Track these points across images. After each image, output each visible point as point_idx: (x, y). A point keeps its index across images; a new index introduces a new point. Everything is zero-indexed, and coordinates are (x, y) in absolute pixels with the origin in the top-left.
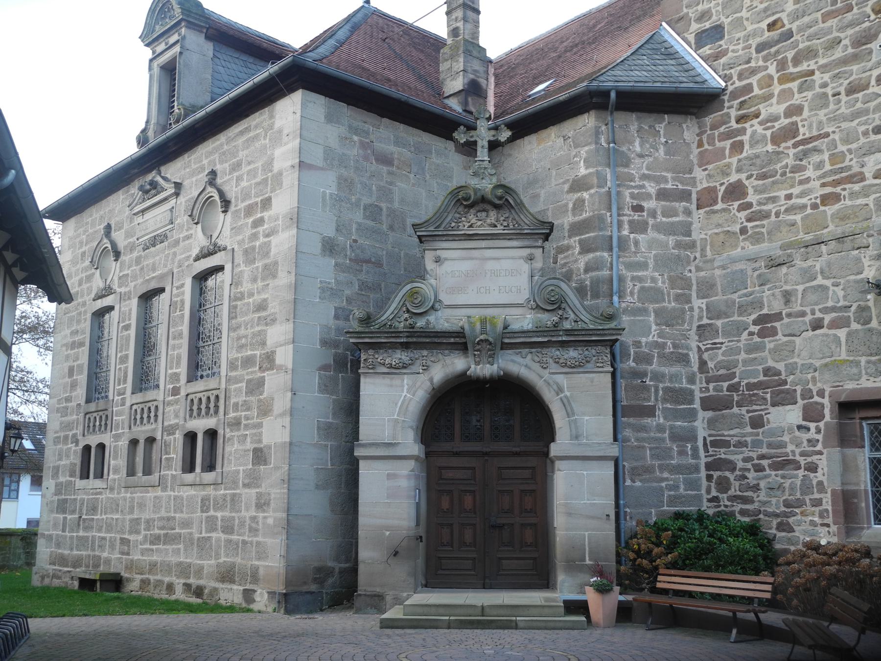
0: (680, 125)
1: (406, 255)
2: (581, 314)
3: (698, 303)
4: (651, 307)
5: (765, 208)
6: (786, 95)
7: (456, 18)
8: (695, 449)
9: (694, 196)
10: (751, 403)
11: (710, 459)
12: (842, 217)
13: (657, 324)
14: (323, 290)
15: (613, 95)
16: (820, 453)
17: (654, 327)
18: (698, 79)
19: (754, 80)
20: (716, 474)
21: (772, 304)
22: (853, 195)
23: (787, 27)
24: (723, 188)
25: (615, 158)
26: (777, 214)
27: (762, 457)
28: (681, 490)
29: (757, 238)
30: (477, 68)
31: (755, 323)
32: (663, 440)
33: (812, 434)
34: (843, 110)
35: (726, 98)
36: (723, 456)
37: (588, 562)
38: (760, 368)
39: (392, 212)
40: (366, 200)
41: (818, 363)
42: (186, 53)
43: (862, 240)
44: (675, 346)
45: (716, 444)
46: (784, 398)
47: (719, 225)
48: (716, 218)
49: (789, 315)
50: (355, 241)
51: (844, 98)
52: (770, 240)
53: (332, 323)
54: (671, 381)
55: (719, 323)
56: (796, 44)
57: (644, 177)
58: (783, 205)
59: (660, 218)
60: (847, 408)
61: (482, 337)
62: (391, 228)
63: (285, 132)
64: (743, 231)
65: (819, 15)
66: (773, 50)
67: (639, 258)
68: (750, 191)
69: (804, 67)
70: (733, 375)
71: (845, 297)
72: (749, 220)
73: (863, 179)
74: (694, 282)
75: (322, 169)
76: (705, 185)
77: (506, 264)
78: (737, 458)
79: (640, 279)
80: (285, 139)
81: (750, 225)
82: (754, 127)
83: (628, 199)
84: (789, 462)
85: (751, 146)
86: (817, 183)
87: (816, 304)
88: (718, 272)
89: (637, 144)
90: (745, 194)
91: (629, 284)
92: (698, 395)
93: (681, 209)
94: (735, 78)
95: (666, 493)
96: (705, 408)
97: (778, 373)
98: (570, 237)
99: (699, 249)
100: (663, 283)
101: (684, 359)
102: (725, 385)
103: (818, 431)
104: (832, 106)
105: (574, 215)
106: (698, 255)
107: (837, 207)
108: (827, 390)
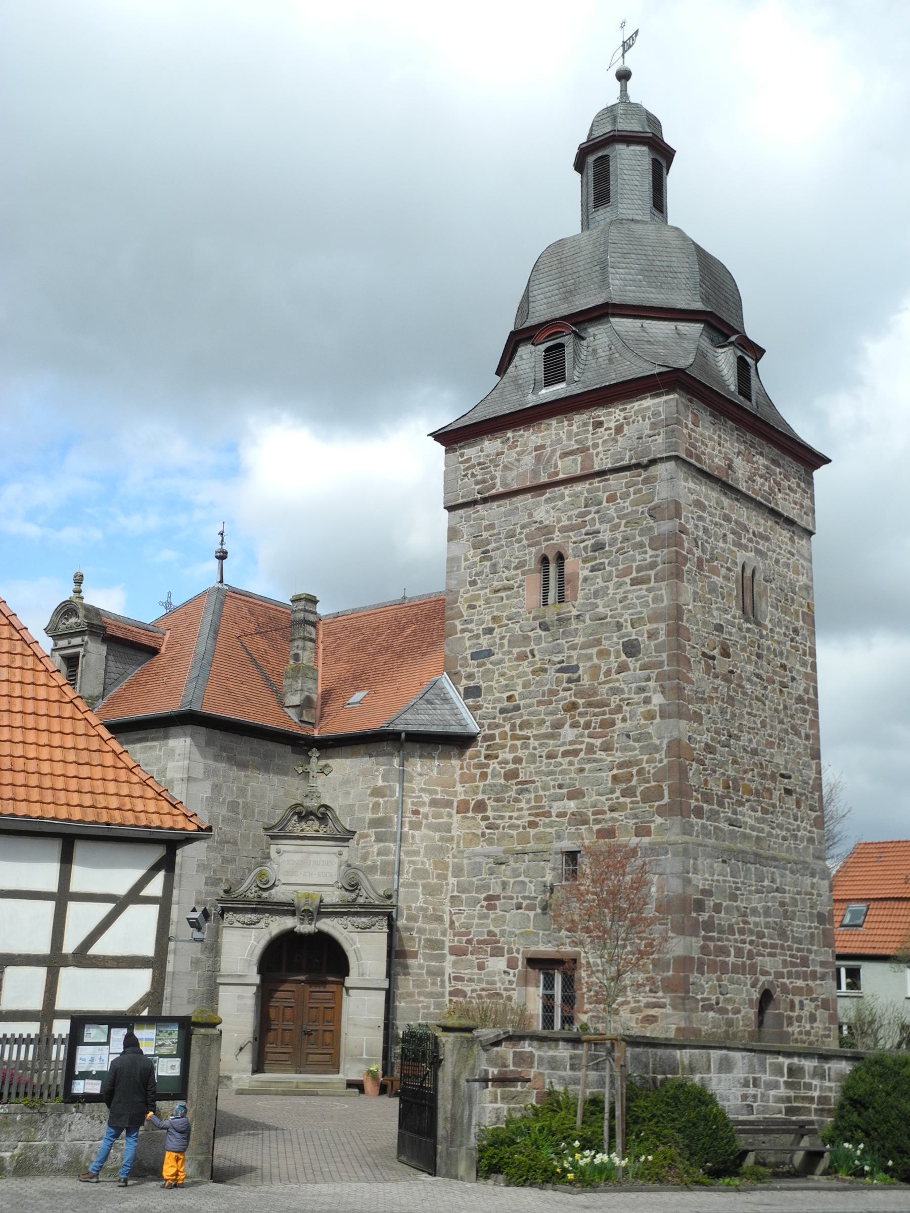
0: (449, 753)
1: (254, 835)
2: (371, 892)
3: (452, 880)
4: (420, 882)
5: (497, 822)
6: (513, 748)
7: (298, 647)
8: (443, 982)
9: (455, 804)
10: (479, 953)
11: (452, 989)
12: (539, 838)
13: (423, 894)
14: (199, 866)
15: (403, 735)
16: (514, 990)
17: (421, 896)
18: (463, 722)
19: (497, 732)
20: (455, 999)
21: (496, 890)
22: (546, 825)
23: (518, 702)
24: (473, 802)
25: (403, 776)
26: (504, 828)
27: (483, 990)
28: (432, 1009)
29: (490, 842)
30: (310, 686)
31: (485, 899)
32: (422, 975)
33: (511, 977)
34: (543, 768)
35: (479, 739)
36: (460, 987)
37: (364, 1056)
38: (485, 930)
39: (246, 805)
40: (229, 799)
41: (517, 932)
42: (88, 655)
43: (546, 856)
44: (434, 910)
45: (457, 979)
46: (497, 952)
47: (469, 828)
48: (467, 822)
49: (504, 898)
50: (221, 829)
51: (544, 759)
52: (498, 845)
53: (203, 888)
54: (430, 934)
55: (464, 896)
56: (521, 716)
57: (422, 790)
58: (506, 822)
59: (431, 820)
60: (533, 962)
61: (306, 908)
62: (245, 817)
63: (177, 752)
64: (483, 834)
65: (535, 700)
66: (509, 715)
67: (414, 848)
68: (489, 808)
69: (524, 733)
70: (469, 933)
71: (535, 891)
72: (487, 828)
73: (551, 816)
74: (451, 865)
75: (201, 780)
76: (463, 798)
77: (324, 857)
78: (468, 989)
79: (414, 863)
80: (177, 757)
81: (488, 831)
82: (494, 764)
83: (410, 806)
84: (498, 994)
85: (492, 778)
86: (527, 813)
87: (520, 893)
88: (466, 861)
89: (418, 766)
90: (485, 810)
91: (406, 866)
92: (447, 944)
93: (445, 814)
94: (486, 727)
95: (421, 1011)
96: (451, 954)
97: (495, 935)
98: (369, 828)
99: (455, 841)
100: (430, 865)
101: (440, 919)
102: (465, 939)
103: (514, 976)
104: (538, 764)
105: (373, 813)
106: (455, 846)
107: (536, 830)
108: (521, 949)
